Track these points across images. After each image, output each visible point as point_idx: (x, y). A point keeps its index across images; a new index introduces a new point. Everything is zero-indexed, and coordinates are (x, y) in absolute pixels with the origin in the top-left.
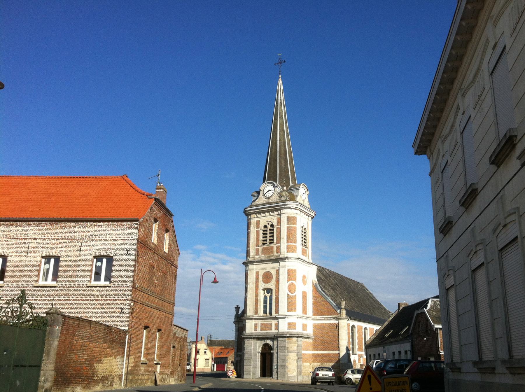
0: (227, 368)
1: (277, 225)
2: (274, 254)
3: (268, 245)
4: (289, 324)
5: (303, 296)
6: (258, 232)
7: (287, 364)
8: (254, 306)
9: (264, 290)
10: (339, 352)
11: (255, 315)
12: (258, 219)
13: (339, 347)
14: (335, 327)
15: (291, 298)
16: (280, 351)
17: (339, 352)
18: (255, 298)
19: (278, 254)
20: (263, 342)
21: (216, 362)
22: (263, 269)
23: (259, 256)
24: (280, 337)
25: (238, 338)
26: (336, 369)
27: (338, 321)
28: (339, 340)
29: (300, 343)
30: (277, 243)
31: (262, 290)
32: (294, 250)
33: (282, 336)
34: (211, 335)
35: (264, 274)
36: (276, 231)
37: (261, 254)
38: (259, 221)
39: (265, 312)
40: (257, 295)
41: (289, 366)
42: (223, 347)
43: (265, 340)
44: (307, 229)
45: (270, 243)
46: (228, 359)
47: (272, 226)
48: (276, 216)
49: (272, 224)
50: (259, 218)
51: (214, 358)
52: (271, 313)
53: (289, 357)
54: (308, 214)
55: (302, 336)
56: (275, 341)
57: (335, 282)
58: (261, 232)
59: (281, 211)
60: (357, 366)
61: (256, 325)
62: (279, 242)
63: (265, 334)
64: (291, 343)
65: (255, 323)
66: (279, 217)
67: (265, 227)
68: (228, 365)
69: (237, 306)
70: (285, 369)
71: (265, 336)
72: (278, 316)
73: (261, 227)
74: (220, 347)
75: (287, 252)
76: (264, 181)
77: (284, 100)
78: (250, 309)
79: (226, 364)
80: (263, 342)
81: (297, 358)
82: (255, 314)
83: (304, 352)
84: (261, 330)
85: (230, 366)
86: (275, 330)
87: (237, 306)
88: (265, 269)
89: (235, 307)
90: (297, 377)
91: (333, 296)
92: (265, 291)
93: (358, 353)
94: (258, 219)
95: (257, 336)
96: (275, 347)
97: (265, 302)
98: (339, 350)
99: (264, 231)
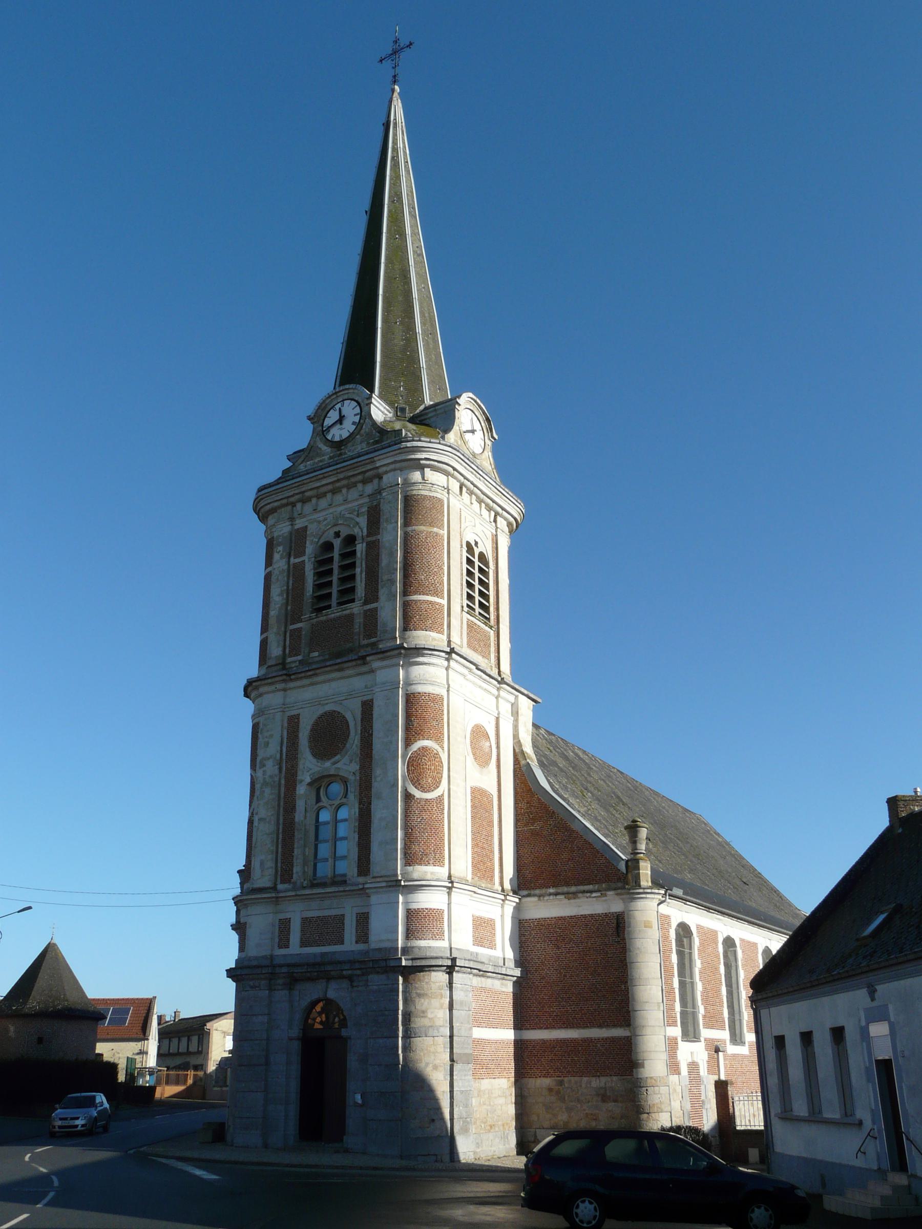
3: (335, 612)
5: (474, 807)
23: (300, 658)
26: (620, 1104)
29: (462, 993)
54: (494, 501)
55: (472, 965)
57: (608, 786)
60: (703, 1087)
67: (328, 547)
77: (408, 152)
78: (262, 863)
84: (304, 943)
86: (357, 942)
89: (239, 872)
91: (599, 821)
93: (706, 1033)
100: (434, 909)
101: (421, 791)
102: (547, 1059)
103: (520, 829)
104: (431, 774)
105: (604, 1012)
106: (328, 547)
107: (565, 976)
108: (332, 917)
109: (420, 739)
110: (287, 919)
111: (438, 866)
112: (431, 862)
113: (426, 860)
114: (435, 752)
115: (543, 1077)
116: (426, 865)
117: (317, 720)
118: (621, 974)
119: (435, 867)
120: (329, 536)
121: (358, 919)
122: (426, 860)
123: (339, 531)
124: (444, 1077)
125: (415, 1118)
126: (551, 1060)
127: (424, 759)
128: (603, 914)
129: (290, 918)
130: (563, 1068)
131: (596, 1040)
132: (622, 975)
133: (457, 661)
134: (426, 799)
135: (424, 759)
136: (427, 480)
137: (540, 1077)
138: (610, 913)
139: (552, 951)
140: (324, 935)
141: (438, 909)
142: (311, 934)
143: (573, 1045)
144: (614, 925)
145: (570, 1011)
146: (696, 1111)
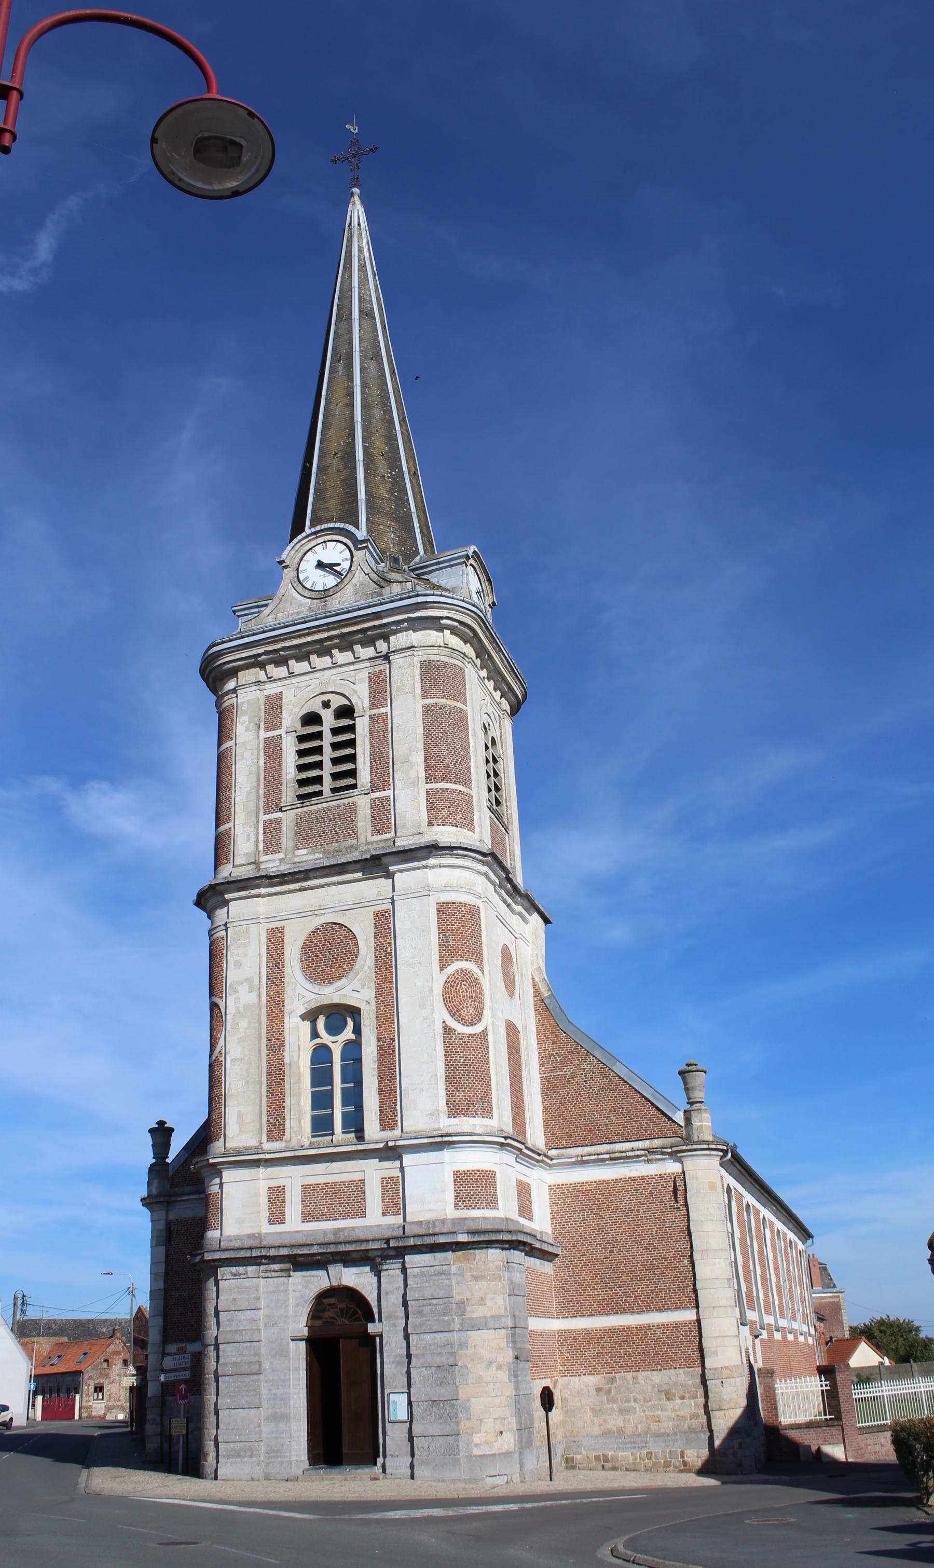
0: (80, 1409)
1: (373, 706)
2: (362, 839)
3: (328, 802)
4: (460, 1178)
6: (273, 749)
7: (462, 1395)
8: (264, 1099)
9: (311, 1016)
10: (698, 1313)
11: (267, 1146)
12: (271, 689)
13: (695, 1291)
14: (669, 1196)
15: (466, 1047)
16: (418, 1321)
17: (698, 1313)
18: (269, 1061)
19: (387, 836)
20: (319, 1281)
21: (40, 1388)
22: (303, 915)
23: (281, 855)
24: (415, 1246)
25: (166, 1273)
27: (682, 1162)
28: (691, 1256)
30: (374, 788)
31: (304, 1017)
32: (464, 818)
33: (428, 1241)
34: (24, 1296)
35: (309, 939)
36: (367, 733)
37: (291, 844)
38: (279, 696)
39: (322, 1125)
40: (276, 1045)
41: (473, 1400)
42: (65, 1339)
43: (331, 1269)
44: (498, 741)
45: (334, 790)
46: (86, 1377)
47: (346, 712)
48: (368, 664)
49: (348, 703)
50: (279, 684)
51: (34, 1375)
52: (355, 1124)
53: (470, 1351)
56: (392, 1271)
58: (290, 748)
59: (392, 638)
61: (277, 1197)
62: (381, 780)
63: (331, 1238)
64: (476, 1278)
65: (274, 1183)
66: (378, 668)
68: (85, 1399)
69: (161, 1123)
70: (453, 1417)
71: (332, 1249)
72: (401, 1139)
73: (290, 718)
74: (53, 1340)
75: (430, 824)
76: (297, 528)
78: (240, 1116)
79: (78, 1397)
80: (319, 1281)
81: (510, 1354)
82: (270, 1139)
83: (536, 1324)
84: (306, 1218)
85: (90, 1404)
86: (384, 1214)
87: (161, 1123)
88: (313, 913)
90: (516, 1456)
92: (321, 1022)
94: (271, 689)
95: (284, 1252)
96: (391, 1302)
97: (321, 1076)
98: (697, 1307)
99: (301, 739)
100: (487, 1171)
101: (462, 1024)
102: (592, 1352)
103: (545, 1075)
104: (473, 1003)
105: (663, 1293)
106: (312, 719)
107: (612, 1252)
108: (347, 1183)
109: (458, 960)
110: (280, 1187)
111: (487, 1117)
112: (479, 1113)
113: (473, 1110)
114: (475, 976)
115: (588, 1374)
116: (474, 1117)
117: (310, 935)
118: (682, 1247)
119: (483, 1119)
120: (315, 706)
121: (385, 1184)
122: (473, 1110)
123: (329, 701)
124: (509, 1378)
125: (480, 1430)
126: (597, 1353)
127: (464, 985)
128: (657, 1175)
129: (284, 1186)
130: (614, 1362)
131: (654, 1326)
132: (685, 1248)
133: (400, 871)
134: (469, 1035)
135: (464, 985)
136: (382, 652)
137: (585, 1375)
138: (665, 1174)
139: (593, 1222)
140: (336, 1206)
141: (490, 1171)
142: (317, 1206)
143: (625, 1334)
144: (671, 1189)
145: (620, 1294)
146: (902, 1401)
